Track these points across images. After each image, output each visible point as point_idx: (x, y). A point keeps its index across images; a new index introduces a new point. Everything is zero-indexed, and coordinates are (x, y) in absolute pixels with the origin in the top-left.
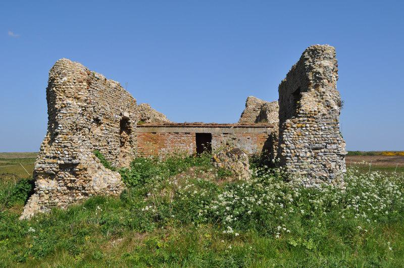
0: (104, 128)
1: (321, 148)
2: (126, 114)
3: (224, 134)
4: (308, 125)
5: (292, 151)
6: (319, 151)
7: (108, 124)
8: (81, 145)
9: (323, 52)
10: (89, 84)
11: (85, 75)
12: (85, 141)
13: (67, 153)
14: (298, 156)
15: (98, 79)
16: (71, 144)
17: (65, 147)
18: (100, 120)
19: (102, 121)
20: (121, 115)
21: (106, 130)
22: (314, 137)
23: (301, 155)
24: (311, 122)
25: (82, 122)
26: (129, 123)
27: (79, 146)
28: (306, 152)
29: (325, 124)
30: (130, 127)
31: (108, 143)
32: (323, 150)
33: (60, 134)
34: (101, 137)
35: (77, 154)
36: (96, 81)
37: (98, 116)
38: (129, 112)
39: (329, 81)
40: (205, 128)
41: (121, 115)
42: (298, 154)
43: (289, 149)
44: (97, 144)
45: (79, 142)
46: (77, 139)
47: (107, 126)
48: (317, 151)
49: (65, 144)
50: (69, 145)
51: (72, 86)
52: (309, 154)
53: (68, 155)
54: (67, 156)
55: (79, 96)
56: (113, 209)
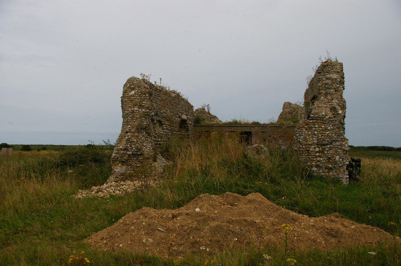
0: (165, 128)
1: (327, 145)
2: (184, 117)
3: (262, 132)
4: (317, 126)
5: (304, 146)
6: (326, 147)
7: (168, 125)
8: (144, 140)
9: (332, 67)
10: (151, 94)
11: (147, 88)
12: (147, 137)
13: (134, 146)
14: (308, 151)
15: (160, 91)
16: (137, 139)
17: (133, 142)
18: (162, 122)
19: (163, 123)
20: (180, 117)
21: (167, 129)
22: (322, 136)
23: (311, 150)
24: (319, 124)
25: (145, 123)
26: (187, 124)
27: (143, 142)
28: (315, 148)
29: (331, 125)
30: (187, 127)
31: (169, 139)
32: (328, 146)
33: (130, 132)
34: (163, 134)
35: (141, 147)
36: (159, 92)
37: (160, 119)
38: (187, 115)
39: (336, 91)
40: (244, 128)
41: (180, 117)
42: (308, 149)
43: (301, 145)
44: (160, 140)
45: (143, 138)
46: (141, 136)
47: (167, 126)
48: (324, 147)
49: (132, 140)
50: (135, 140)
51: (138, 97)
52: (317, 149)
53: (135, 147)
54: (134, 148)
55: (143, 105)
56: (178, 196)
